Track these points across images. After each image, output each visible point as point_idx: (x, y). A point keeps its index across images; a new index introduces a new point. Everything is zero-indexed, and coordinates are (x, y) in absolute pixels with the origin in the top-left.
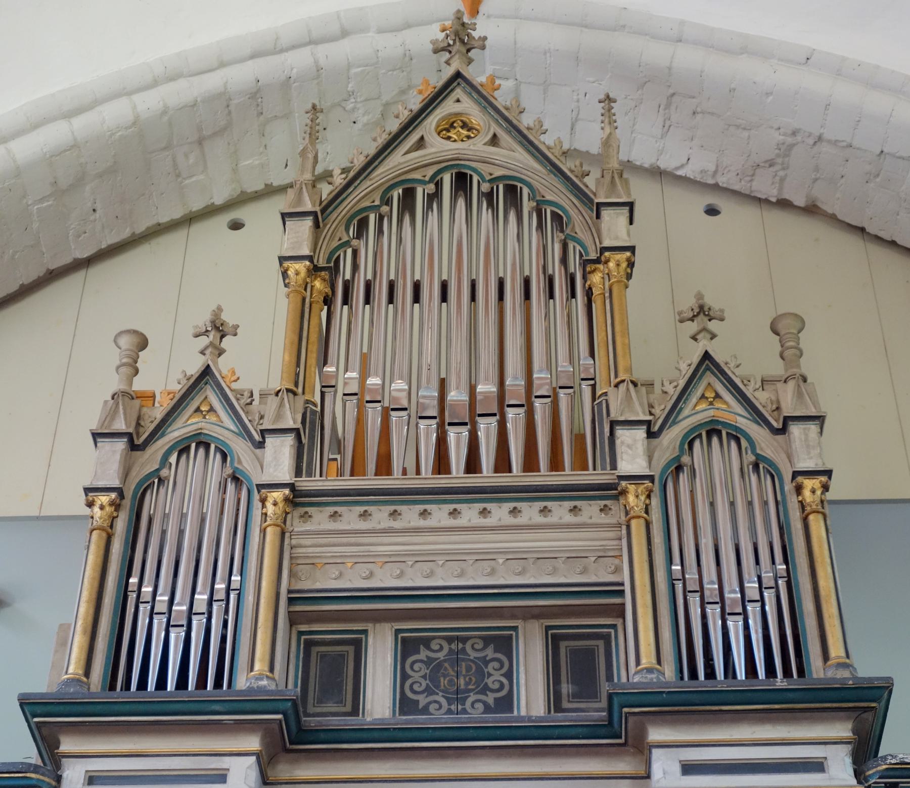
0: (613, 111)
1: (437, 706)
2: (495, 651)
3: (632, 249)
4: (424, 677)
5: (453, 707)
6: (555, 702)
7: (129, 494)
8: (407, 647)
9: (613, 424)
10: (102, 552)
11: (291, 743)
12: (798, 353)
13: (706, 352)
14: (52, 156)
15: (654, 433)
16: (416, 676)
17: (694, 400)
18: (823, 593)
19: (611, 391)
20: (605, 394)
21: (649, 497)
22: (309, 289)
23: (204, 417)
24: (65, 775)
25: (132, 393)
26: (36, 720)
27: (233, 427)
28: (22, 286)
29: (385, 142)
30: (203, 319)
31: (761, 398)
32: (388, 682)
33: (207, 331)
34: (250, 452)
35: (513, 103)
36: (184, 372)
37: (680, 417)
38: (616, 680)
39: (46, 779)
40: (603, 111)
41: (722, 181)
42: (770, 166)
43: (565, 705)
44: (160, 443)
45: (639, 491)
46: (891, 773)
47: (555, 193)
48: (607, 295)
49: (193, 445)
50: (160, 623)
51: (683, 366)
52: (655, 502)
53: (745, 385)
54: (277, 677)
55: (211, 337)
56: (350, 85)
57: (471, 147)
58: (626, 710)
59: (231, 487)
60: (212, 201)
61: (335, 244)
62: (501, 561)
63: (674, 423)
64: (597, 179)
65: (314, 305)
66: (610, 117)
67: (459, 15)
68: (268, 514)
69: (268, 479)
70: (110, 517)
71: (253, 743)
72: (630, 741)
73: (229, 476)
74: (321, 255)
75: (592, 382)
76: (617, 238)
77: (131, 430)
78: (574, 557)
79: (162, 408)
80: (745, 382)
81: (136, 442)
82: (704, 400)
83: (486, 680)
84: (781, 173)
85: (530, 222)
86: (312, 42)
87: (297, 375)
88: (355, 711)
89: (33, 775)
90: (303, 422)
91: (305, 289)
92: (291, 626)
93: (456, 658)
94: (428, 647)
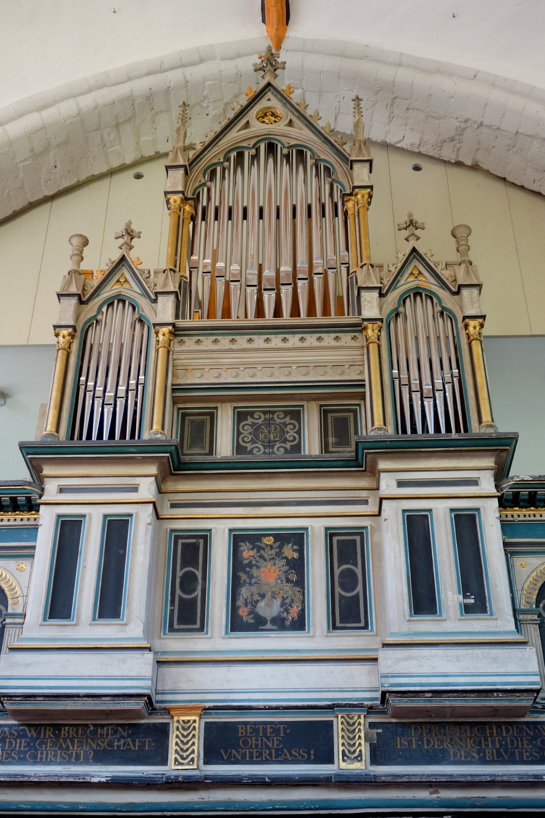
0: (360, 106)
1: (257, 450)
2: (291, 419)
3: (371, 187)
4: (250, 433)
5: (267, 450)
6: (325, 447)
7: (79, 329)
8: (240, 417)
9: (360, 289)
13: (414, 248)
15: (383, 294)
19: (358, 270)
20: (355, 272)
21: (380, 331)
23: (122, 285)
24: (46, 487)
26: (29, 456)
27: (139, 291)
30: (121, 228)
31: (445, 274)
33: (123, 235)
34: (149, 305)
36: (110, 259)
37: (399, 285)
38: (360, 434)
39: (36, 490)
41: (423, 150)
42: (452, 141)
44: (96, 300)
45: (375, 327)
47: (326, 154)
48: (356, 214)
49: (116, 302)
50: (98, 403)
51: (400, 256)
52: (384, 334)
54: (166, 433)
55: (125, 239)
56: (205, 92)
57: (277, 127)
58: (366, 451)
59: (138, 326)
60: (124, 162)
61: (197, 184)
62: (294, 368)
63: (395, 288)
64: (351, 146)
65: (185, 220)
66: (358, 109)
68: (160, 340)
70: (68, 342)
71: (153, 469)
72: (368, 469)
73: (137, 319)
75: (347, 265)
76: (362, 181)
77: (80, 292)
80: (436, 265)
84: (458, 145)
85: (311, 172)
86: (183, 66)
87: (176, 261)
88: (211, 453)
89: (28, 487)
91: (180, 211)
92: (174, 405)
93: (268, 423)
94: (252, 417)
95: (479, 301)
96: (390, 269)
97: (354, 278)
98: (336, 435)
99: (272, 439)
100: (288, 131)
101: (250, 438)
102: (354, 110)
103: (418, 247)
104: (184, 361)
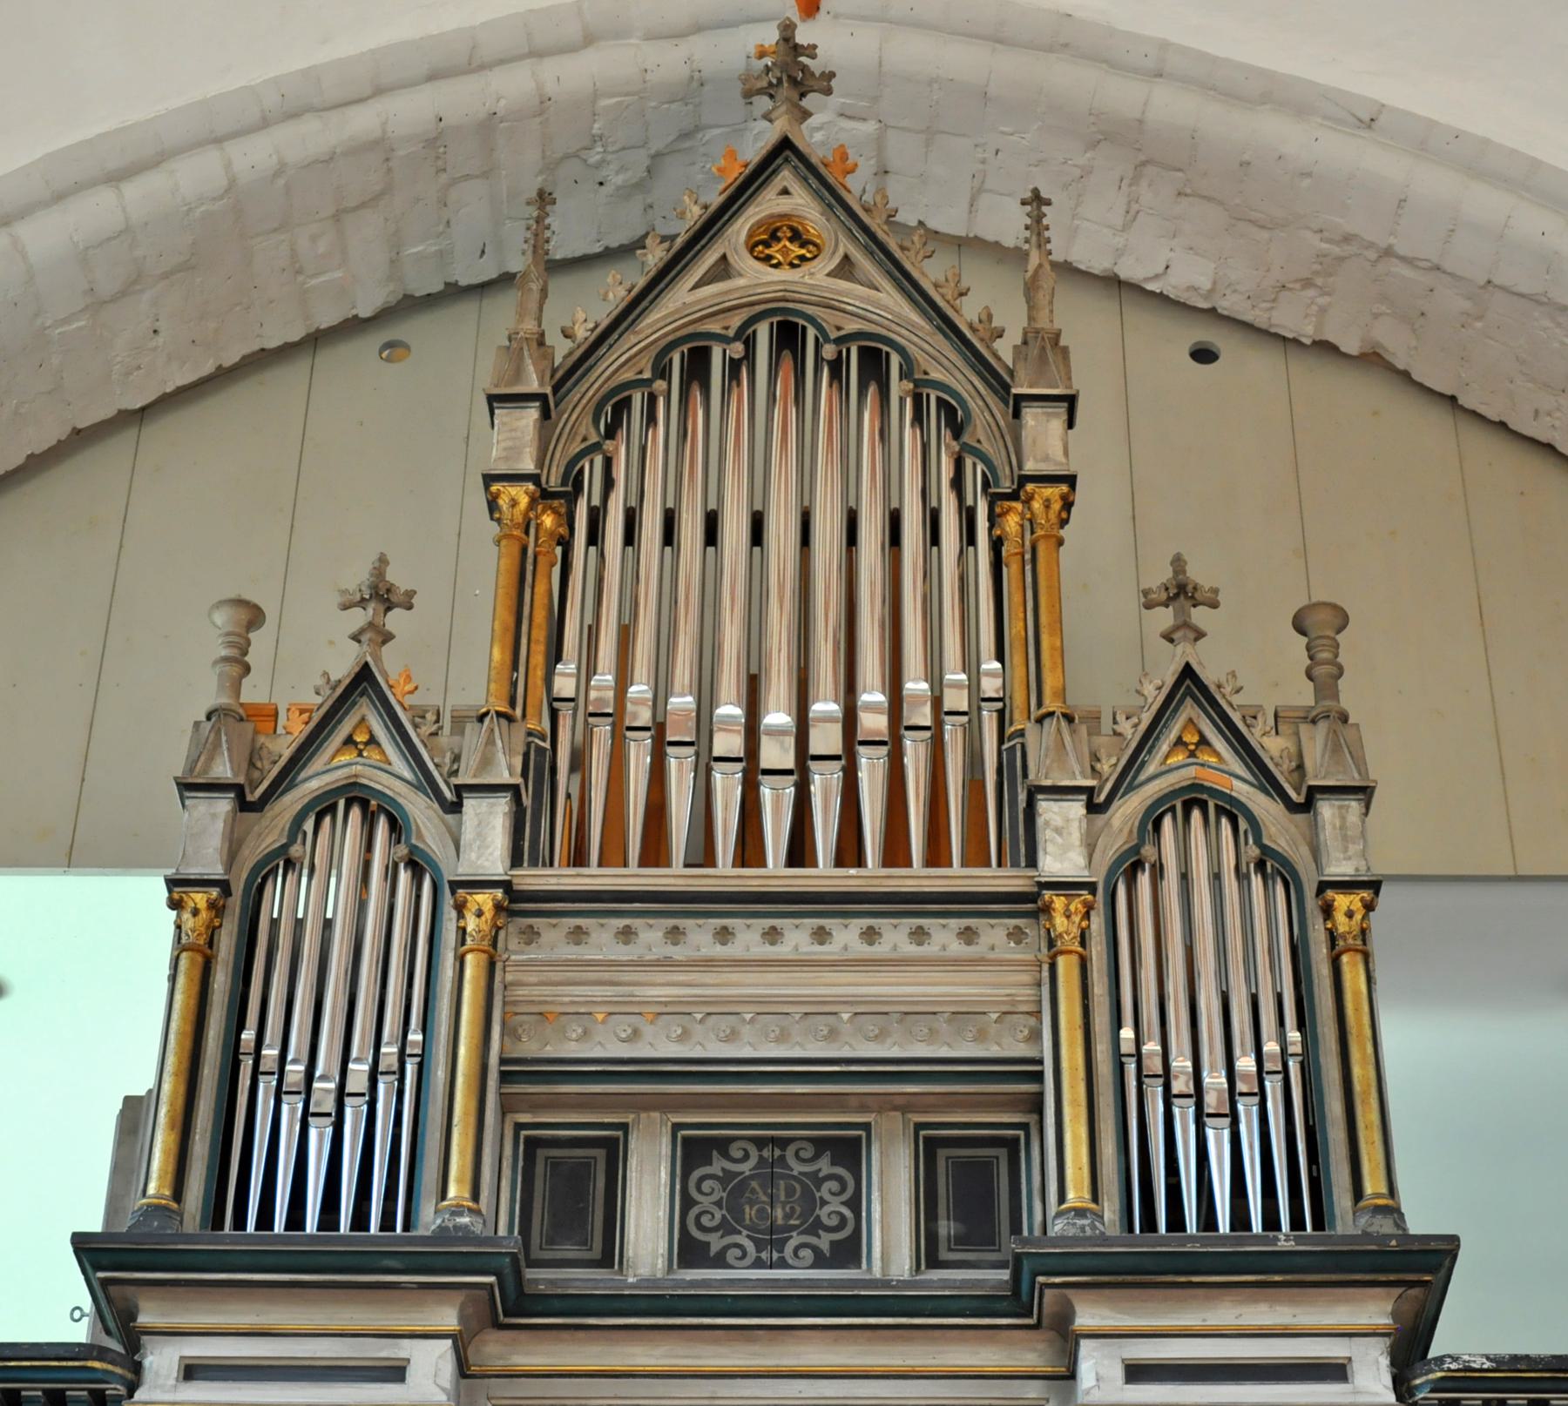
0: (1045, 221)
1: (738, 1252)
2: (833, 1163)
3: (1071, 480)
4: (718, 1204)
5: (764, 1255)
6: (929, 1254)
7: (238, 889)
8: (693, 1152)
9: (1034, 792)
10: (196, 989)
11: (506, 1315)
12: (1334, 670)
13: (1188, 665)
14: (87, 248)
15: (1099, 805)
16: (705, 1202)
17: (1165, 747)
18: (1357, 1087)
19: (1030, 727)
20: (1021, 733)
21: (1087, 916)
22: (532, 531)
23: (360, 755)
24: (147, 1363)
25: (241, 711)
26: (101, 1275)
27: (408, 775)
28: (31, 457)
29: (661, 265)
30: (357, 577)
31: (1273, 747)
32: (663, 1213)
33: (363, 600)
34: (437, 821)
35: (878, 199)
36: (325, 674)
37: (1142, 777)
38: (1025, 1233)
39: (118, 1370)
40: (1028, 221)
41: (1225, 305)
42: (1304, 287)
43: (944, 1255)
44: (288, 798)
45: (1072, 908)
46: (1450, 1385)
47: (946, 368)
48: (1028, 556)
49: (341, 804)
50: (293, 1111)
51: (1149, 690)
52: (1097, 923)
53: (1248, 726)
54: (484, 1211)
55: (370, 611)
56: (596, 126)
57: (807, 279)
58: (1041, 1279)
59: (404, 877)
60: (354, 312)
61: (576, 447)
62: (845, 1016)
63: (1131, 788)
64: (1015, 347)
65: (540, 558)
66: (1039, 234)
67: (789, 33)
68: (469, 929)
69: (471, 871)
70: (208, 927)
71: (447, 1317)
72: (1045, 1322)
73: (401, 859)
74: (554, 469)
75: (999, 705)
76: (1046, 459)
77: (241, 780)
78: (963, 1015)
79: (290, 738)
80: (1249, 721)
81: (250, 798)
82: (1181, 748)
83: (817, 1211)
84: (1322, 301)
86: (537, 54)
87: (514, 684)
89: (97, 1364)
90: (525, 774)
91: (527, 533)
92: (504, 1114)
93: (770, 1172)
94: (726, 1155)
95: (1363, 834)
96: (1118, 728)
97: (1019, 754)
98: (960, 1215)
99: (780, 1222)
100: (839, 293)
101: (718, 1216)
102: (1028, 233)
103: (1200, 663)
104: (537, 991)
